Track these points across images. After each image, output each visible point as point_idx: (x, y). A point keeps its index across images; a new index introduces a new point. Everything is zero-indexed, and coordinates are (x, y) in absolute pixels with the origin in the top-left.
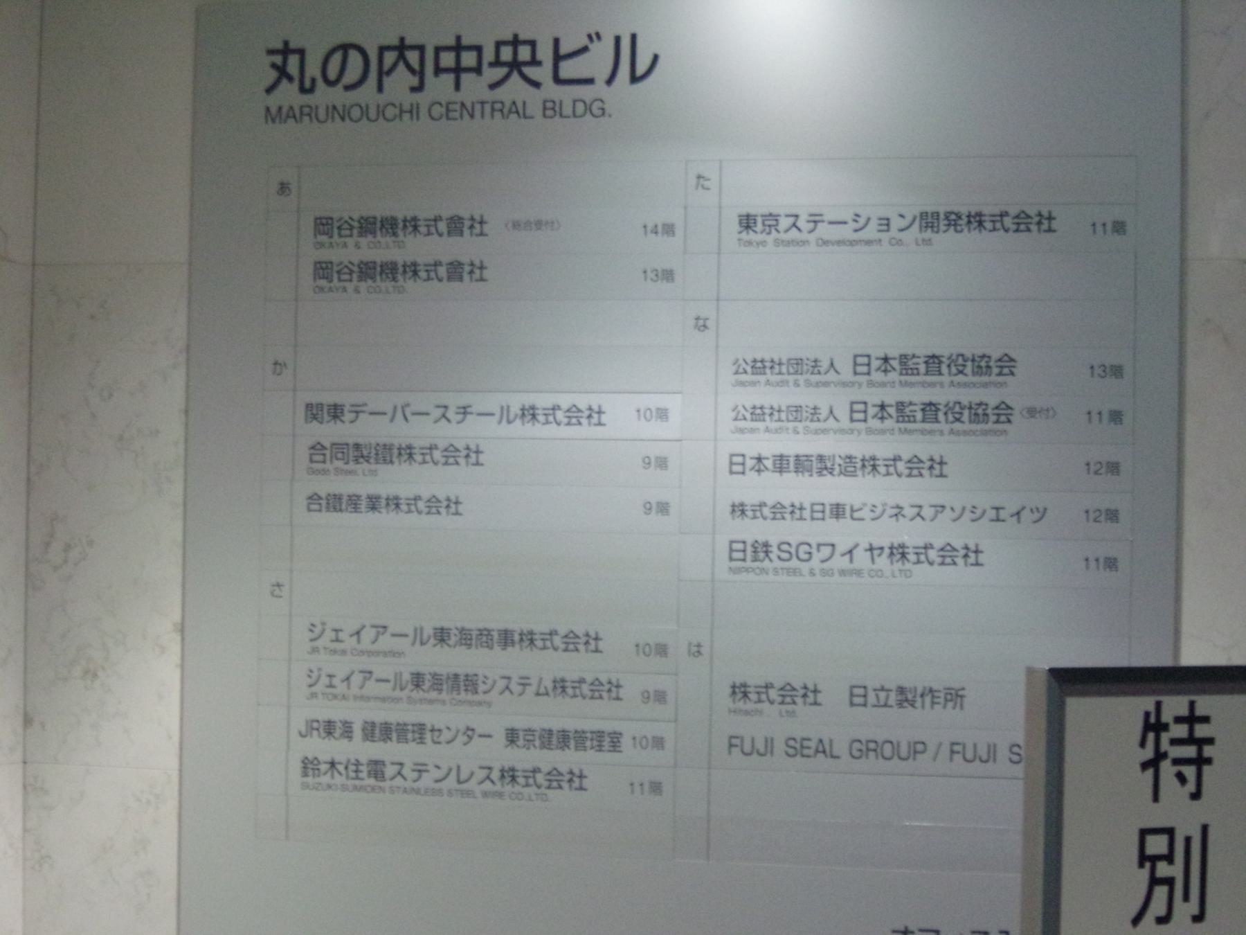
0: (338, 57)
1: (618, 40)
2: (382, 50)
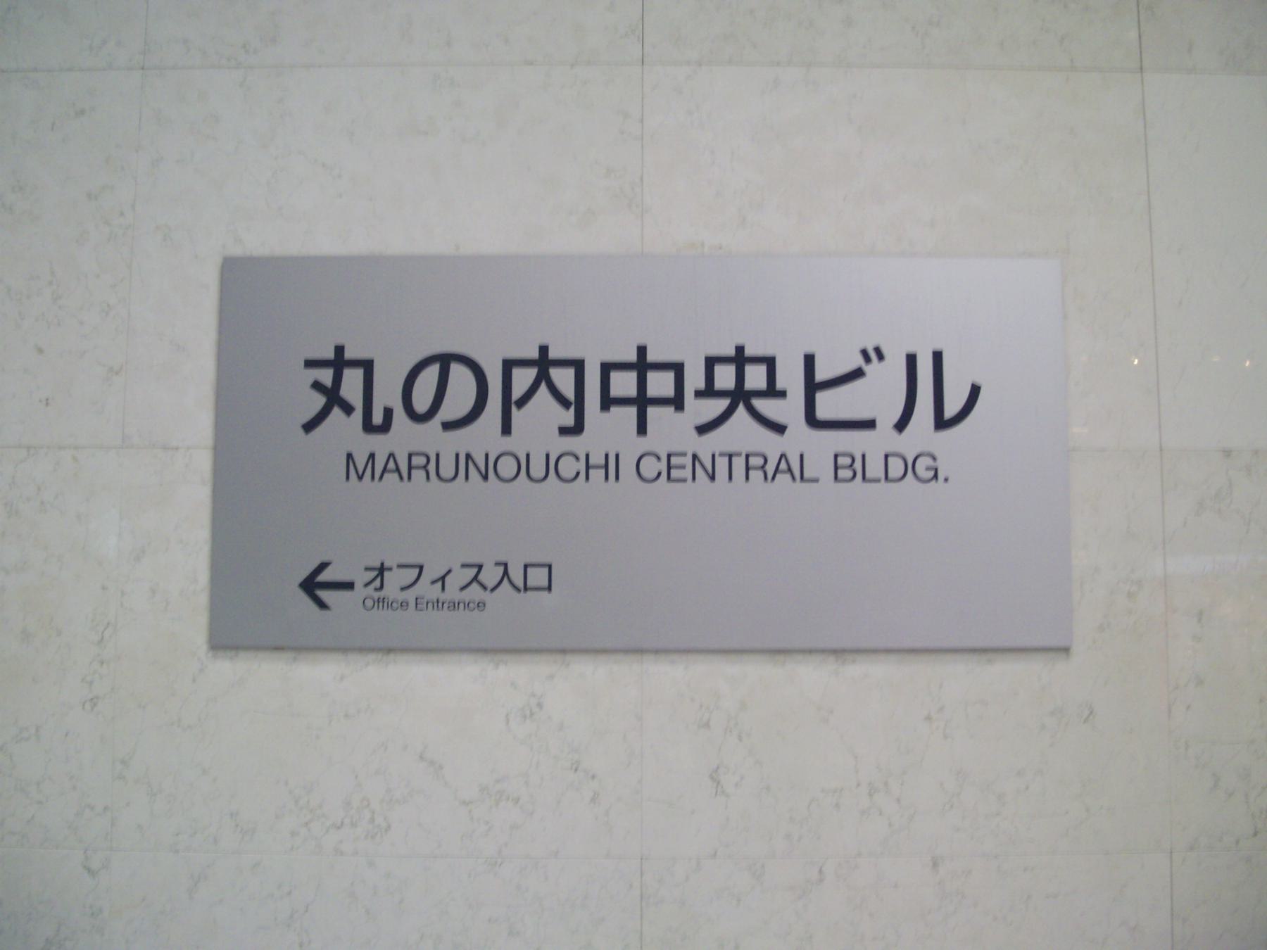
1: (911, 360)
2: (508, 366)
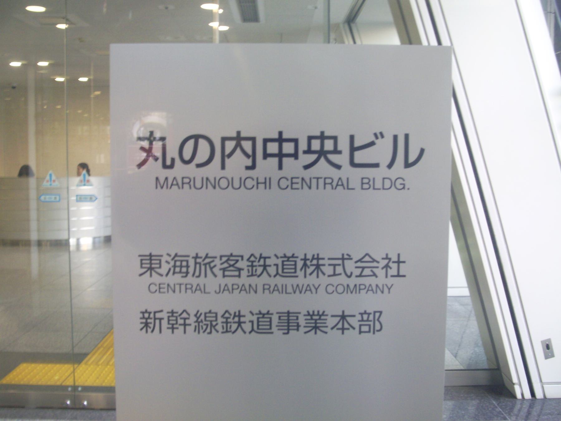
0: (191, 142)
1: (395, 138)
